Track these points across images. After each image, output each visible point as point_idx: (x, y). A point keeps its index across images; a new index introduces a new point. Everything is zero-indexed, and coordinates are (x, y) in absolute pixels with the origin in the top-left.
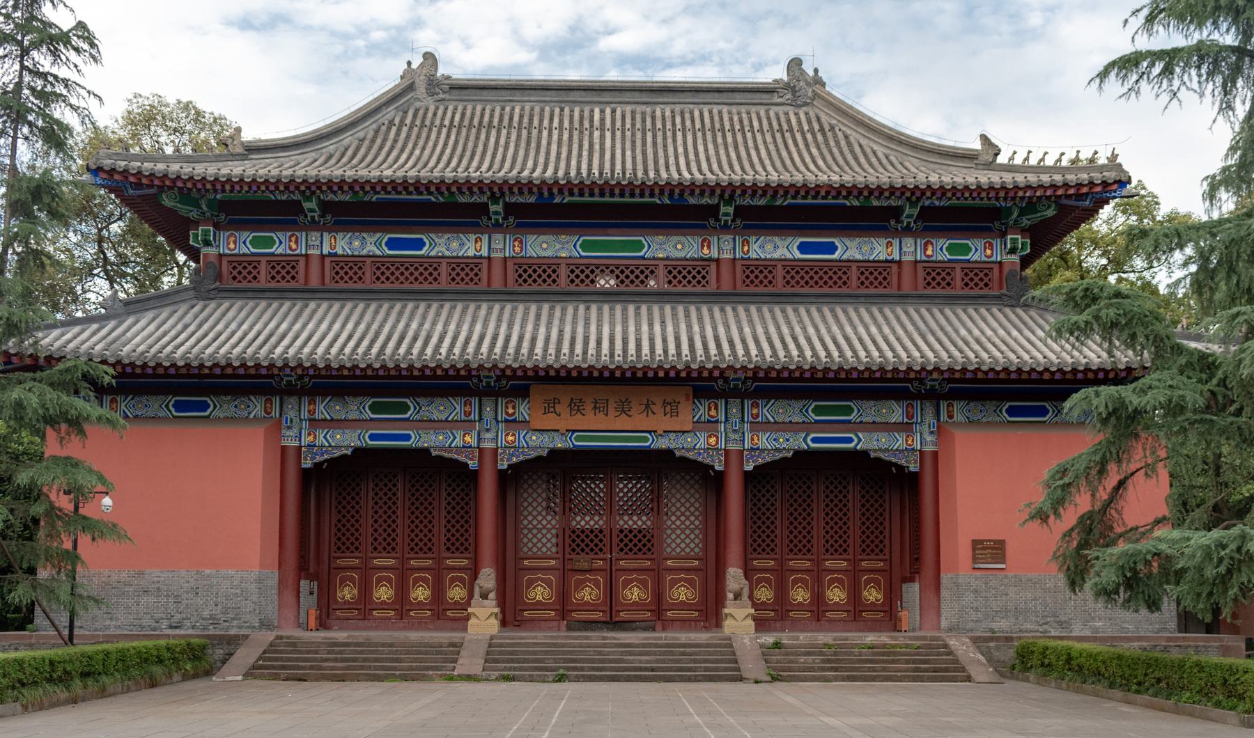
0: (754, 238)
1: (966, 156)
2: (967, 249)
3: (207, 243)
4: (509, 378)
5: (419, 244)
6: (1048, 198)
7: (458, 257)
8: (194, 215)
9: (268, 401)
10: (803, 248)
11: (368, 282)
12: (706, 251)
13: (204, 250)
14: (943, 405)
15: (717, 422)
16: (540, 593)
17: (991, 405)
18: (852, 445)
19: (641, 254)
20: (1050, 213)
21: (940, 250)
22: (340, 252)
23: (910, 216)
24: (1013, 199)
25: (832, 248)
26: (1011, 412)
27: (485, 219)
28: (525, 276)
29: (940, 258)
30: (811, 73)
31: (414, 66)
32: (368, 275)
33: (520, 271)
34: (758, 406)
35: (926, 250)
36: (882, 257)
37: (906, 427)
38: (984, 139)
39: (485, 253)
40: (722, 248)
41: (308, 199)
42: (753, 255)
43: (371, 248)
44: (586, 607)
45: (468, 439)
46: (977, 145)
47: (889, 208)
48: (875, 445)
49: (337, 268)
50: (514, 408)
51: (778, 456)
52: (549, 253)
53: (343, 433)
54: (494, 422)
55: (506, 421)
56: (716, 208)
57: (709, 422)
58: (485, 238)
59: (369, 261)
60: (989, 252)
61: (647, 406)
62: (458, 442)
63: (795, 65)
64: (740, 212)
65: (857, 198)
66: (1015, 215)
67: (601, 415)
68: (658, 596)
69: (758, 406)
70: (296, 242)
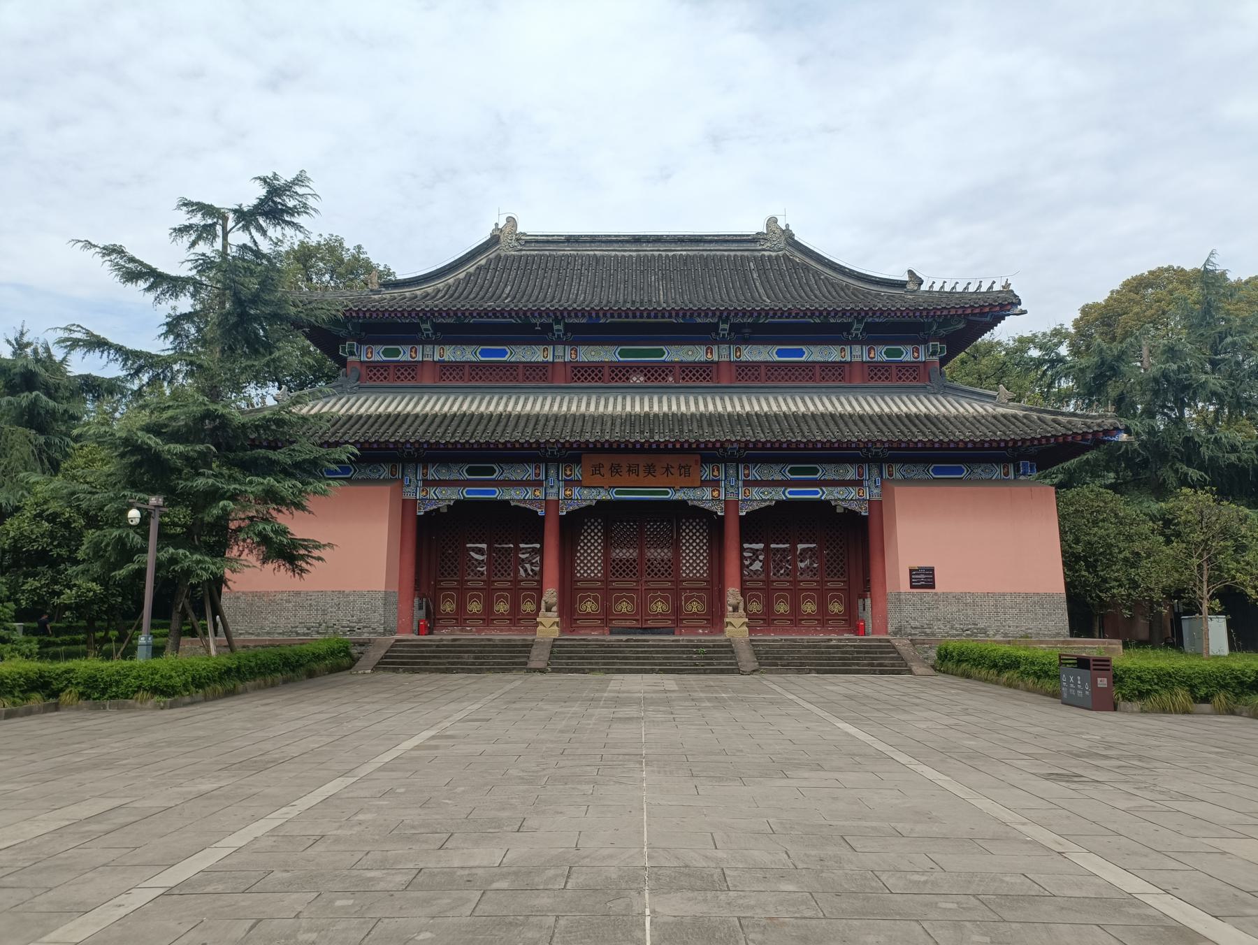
1: (902, 285)
3: (352, 354)
5: (801, 353)
14: (866, 467)
17: (920, 467)
20: (961, 326)
21: (880, 354)
26: (936, 471)
36: (838, 359)
37: (857, 483)
38: (911, 272)
39: (550, 359)
40: (720, 354)
44: (624, 617)
45: (537, 493)
47: (842, 324)
52: (596, 359)
61: (667, 469)
63: (772, 221)
64: (869, 328)
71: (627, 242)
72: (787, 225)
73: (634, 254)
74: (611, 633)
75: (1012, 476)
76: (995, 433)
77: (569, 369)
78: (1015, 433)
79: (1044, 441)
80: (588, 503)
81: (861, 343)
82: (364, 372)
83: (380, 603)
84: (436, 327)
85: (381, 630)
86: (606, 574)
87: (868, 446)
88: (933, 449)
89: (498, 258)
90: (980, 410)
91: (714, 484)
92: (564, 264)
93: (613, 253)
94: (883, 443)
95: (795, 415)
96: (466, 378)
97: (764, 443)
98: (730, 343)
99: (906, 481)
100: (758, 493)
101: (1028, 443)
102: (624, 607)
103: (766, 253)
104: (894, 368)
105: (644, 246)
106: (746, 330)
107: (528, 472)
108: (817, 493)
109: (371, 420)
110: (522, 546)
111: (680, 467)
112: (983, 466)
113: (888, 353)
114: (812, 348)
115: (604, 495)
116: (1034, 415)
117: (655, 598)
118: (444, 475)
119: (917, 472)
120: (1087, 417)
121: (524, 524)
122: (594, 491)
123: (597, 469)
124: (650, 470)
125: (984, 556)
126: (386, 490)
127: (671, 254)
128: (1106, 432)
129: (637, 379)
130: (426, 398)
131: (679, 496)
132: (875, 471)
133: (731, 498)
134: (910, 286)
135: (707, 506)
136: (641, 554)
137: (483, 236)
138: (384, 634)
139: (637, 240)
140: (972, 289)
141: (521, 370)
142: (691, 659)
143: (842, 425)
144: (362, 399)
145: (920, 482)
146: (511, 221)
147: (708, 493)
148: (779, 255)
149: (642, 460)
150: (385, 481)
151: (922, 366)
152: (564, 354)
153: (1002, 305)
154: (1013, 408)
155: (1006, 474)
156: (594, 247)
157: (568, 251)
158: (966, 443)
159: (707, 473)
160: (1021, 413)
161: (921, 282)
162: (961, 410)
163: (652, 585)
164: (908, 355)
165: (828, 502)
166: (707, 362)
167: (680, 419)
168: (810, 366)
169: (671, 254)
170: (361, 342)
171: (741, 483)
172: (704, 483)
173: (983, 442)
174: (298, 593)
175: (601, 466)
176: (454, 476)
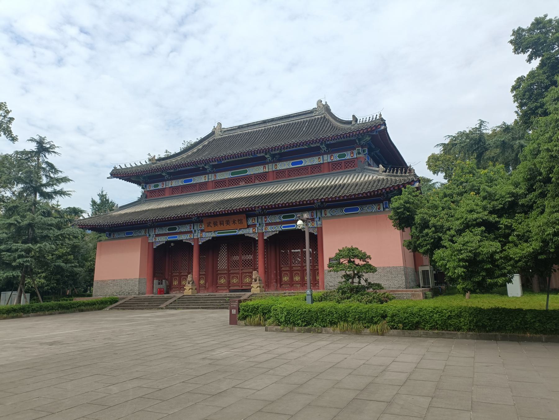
1: (349, 123)
2: (345, 155)
4: (267, 209)
5: (301, 162)
9: (191, 226)
14: (323, 211)
16: (223, 281)
17: (339, 209)
21: (336, 157)
25: (246, 171)
26: (346, 211)
32: (343, 166)
36: (317, 163)
38: (354, 116)
39: (207, 180)
40: (270, 168)
42: (278, 169)
44: (235, 285)
46: (351, 119)
51: (274, 233)
53: (160, 239)
61: (234, 222)
62: (188, 237)
65: (306, 145)
67: (222, 226)
68: (229, 282)
71: (261, 123)
72: (326, 102)
73: (263, 128)
74: (230, 292)
75: (382, 209)
80: (209, 238)
82: (149, 194)
83: (137, 283)
85: (137, 293)
86: (228, 267)
88: (123, 226)
91: (254, 226)
96: (227, 185)
100: (270, 228)
102: (235, 281)
103: (316, 117)
105: (268, 124)
106: (277, 156)
107: (186, 228)
109: (316, 190)
110: (293, 251)
111: (239, 220)
112: (368, 206)
114: (306, 159)
115: (214, 235)
117: (234, 277)
119: (338, 212)
121: (247, 244)
123: (209, 225)
124: (228, 222)
125: (120, 266)
126: (139, 239)
127: (277, 125)
129: (242, 184)
131: (240, 232)
132: (319, 214)
133: (260, 231)
134: (353, 123)
135: (252, 236)
136: (240, 258)
137: (210, 131)
138: (139, 295)
139: (264, 122)
141: (287, 173)
142: (220, 302)
144: (336, 178)
145: (339, 216)
147: (251, 230)
148: (322, 116)
149: (224, 219)
155: (379, 209)
156: (249, 128)
157: (239, 132)
159: (250, 222)
163: (244, 271)
164: (348, 156)
166: (264, 173)
167: (302, 191)
168: (306, 168)
169: (277, 125)
172: (249, 226)
174: (114, 280)
175: (210, 223)
176: (164, 232)
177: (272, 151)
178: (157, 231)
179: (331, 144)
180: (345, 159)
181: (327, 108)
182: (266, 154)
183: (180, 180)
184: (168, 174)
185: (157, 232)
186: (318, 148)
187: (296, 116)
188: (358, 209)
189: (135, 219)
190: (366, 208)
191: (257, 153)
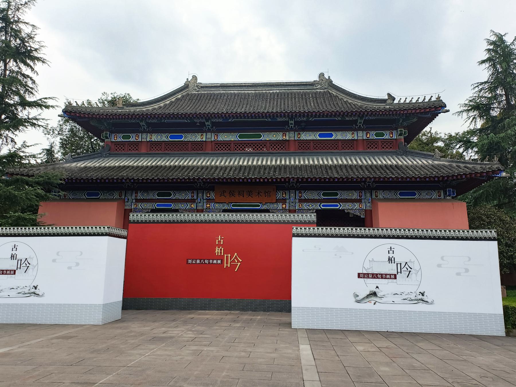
0: (302, 133)
3: (107, 138)
4: (300, 183)
6: (413, 113)
7: (195, 141)
8: (102, 128)
9: (121, 193)
10: (320, 136)
11: (143, 151)
12: (284, 137)
13: (106, 140)
15: (286, 199)
18: (338, 207)
19: (261, 139)
20: (415, 120)
21: (372, 135)
22: (153, 140)
23: (360, 123)
24: (399, 114)
25: (331, 135)
26: (401, 194)
27: (287, 127)
28: (302, 146)
29: (372, 138)
30: (327, 78)
31: (189, 80)
33: (300, 145)
34: (301, 193)
35: (367, 135)
36: (350, 138)
37: (359, 201)
38: (389, 95)
39: (204, 139)
40: (289, 136)
41: (207, 121)
43: (164, 139)
45: (193, 206)
46: (386, 97)
47: (353, 120)
48: (347, 207)
49: (300, 145)
50: (210, 194)
52: (228, 139)
54: (202, 200)
55: (207, 199)
56: (357, 120)
57: (283, 199)
58: (205, 134)
59: (163, 143)
60: (391, 135)
61: (259, 193)
63: (322, 75)
64: (366, 122)
66: (401, 121)
69: (301, 193)
70: (138, 137)
72: (329, 77)
76: (432, 173)
77: (213, 143)
78: (443, 173)
79: (459, 177)
81: (363, 130)
84: (149, 125)
87: (363, 180)
89: (188, 95)
90: (425, 162)
92: (219, 97)
93: (243, 92)
94: (370, 178)
95: (326, 166)
96: (163, 149)
97: (307, 179)
98: (295, 131)
99: (385, 200)
101: (446, 178)
104: (380, 143)
108: (337, 206)
111: (265, 192)
113: (376, 135)
116: (454, 165)
118: (145, 196)
120: (483, 164)
122: (221, 205)
126: (115, 204)
128: (494, 172)
129: (249, 150)
130: (142, 159)
132: (368, 195)
134: (389, 101)
140: (420, 100)
141: (190, 145)
143: (349, 170)
144: (135, 160)
146: (195, 78)
148: (326, 88)
150: (116, 200)
151: (394, 141)
152: (211, 137)
153: (434, 109)
154: (443, 161)
158: (416, 178)
159: (279, 195)
160: (446, 163)
161: (394, 99)
162: (415, 163)
165: (343, 210)
169: (271, 92)
170: (112, 132)
171: (297, 201)
172: (277, 201)
173: (425, 178)
177: (311, 116)
178: (139, 194)
179: (151, 123)
180: (261, 140)
181: (330, 82)
182: (141, 121)
183: (164, 135)
184: (147, 124)
185: (140, 196)
186: (287, 123)
187: (294, 85)
188: (415, 194)
189: (115, 175)
190: (425, 194)
191: (277, 116)
